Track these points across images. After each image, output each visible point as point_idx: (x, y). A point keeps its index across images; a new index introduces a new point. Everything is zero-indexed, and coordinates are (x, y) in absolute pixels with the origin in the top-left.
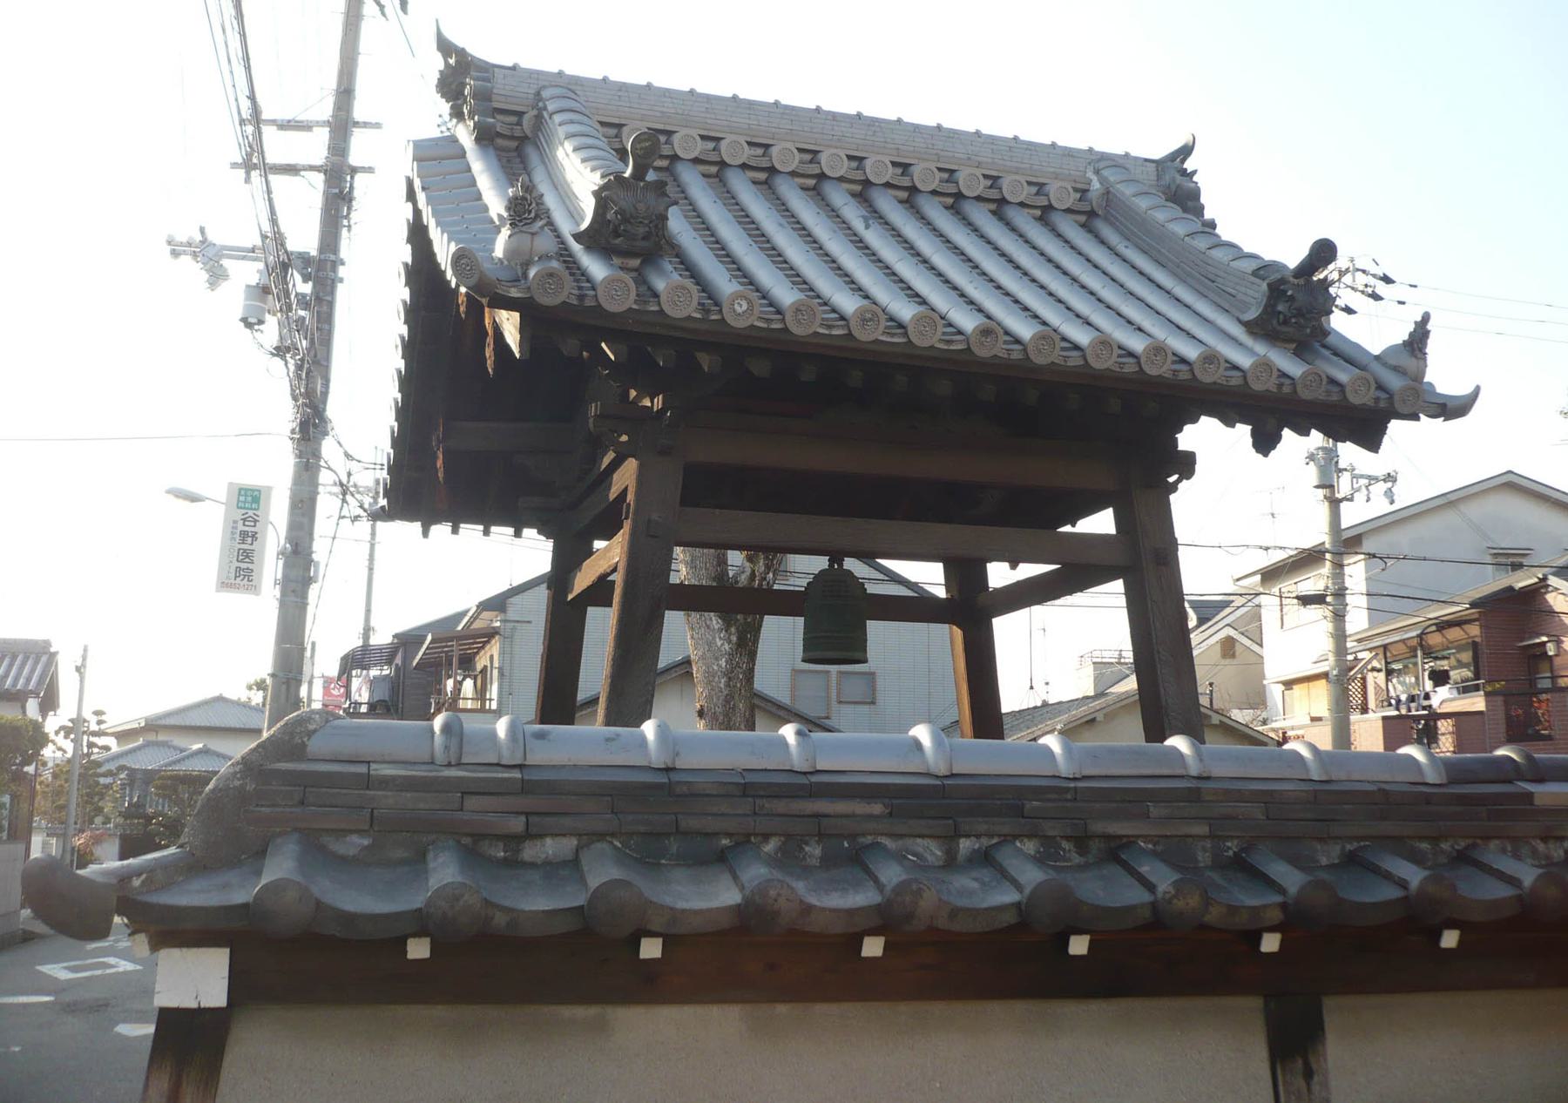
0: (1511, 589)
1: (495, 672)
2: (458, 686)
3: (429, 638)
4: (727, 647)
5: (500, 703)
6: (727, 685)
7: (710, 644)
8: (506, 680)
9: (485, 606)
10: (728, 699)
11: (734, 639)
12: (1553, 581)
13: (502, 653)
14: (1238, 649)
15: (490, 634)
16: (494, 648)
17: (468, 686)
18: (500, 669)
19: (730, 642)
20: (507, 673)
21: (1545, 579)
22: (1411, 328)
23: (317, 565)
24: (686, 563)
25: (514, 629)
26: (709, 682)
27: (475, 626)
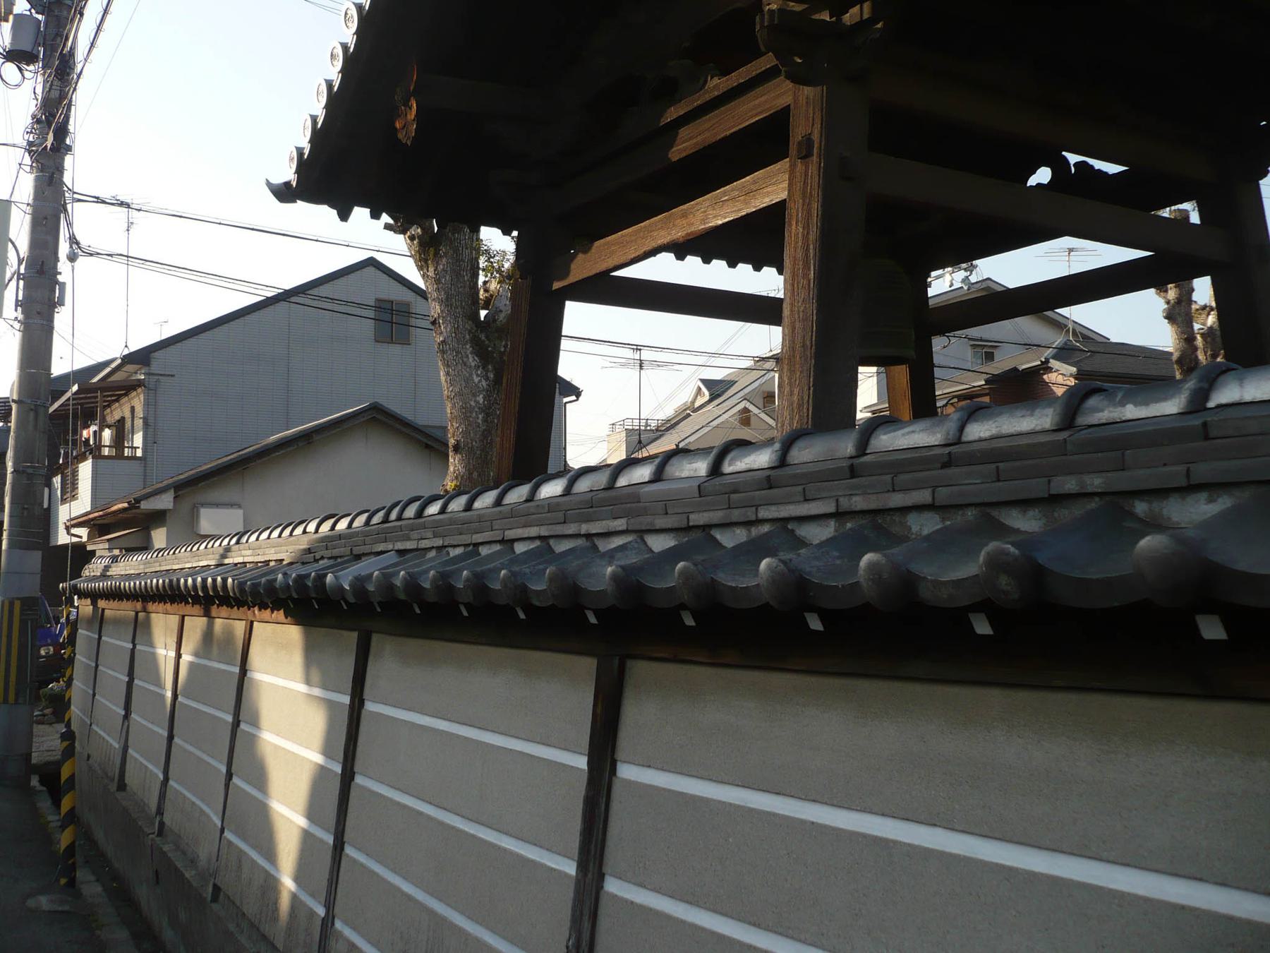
0: (1015, 369)
1: (139, 423)
2: (97, 435)
3: (75, 388)
4: (484, 383)
5: (144, 450)
6: (485, 420)
7: (468, 380)
8: (151, 430)
9: (129, 359)
10: (486, 434)
11: (491, 376)
12: (1054, 364)
13: (147, 404)
14: (753, 419)
15: (129, 388)
16: (137, 400)
17: (107, 434)
18: (145, 420)
19: (487, 379)
20: (151, 421)
21: (1047, 361)
22: (301, 205)
23: (63, 285)
24: (441, 302)
25: (158, 381)
26: (466, 418)
27: (112, 379)
